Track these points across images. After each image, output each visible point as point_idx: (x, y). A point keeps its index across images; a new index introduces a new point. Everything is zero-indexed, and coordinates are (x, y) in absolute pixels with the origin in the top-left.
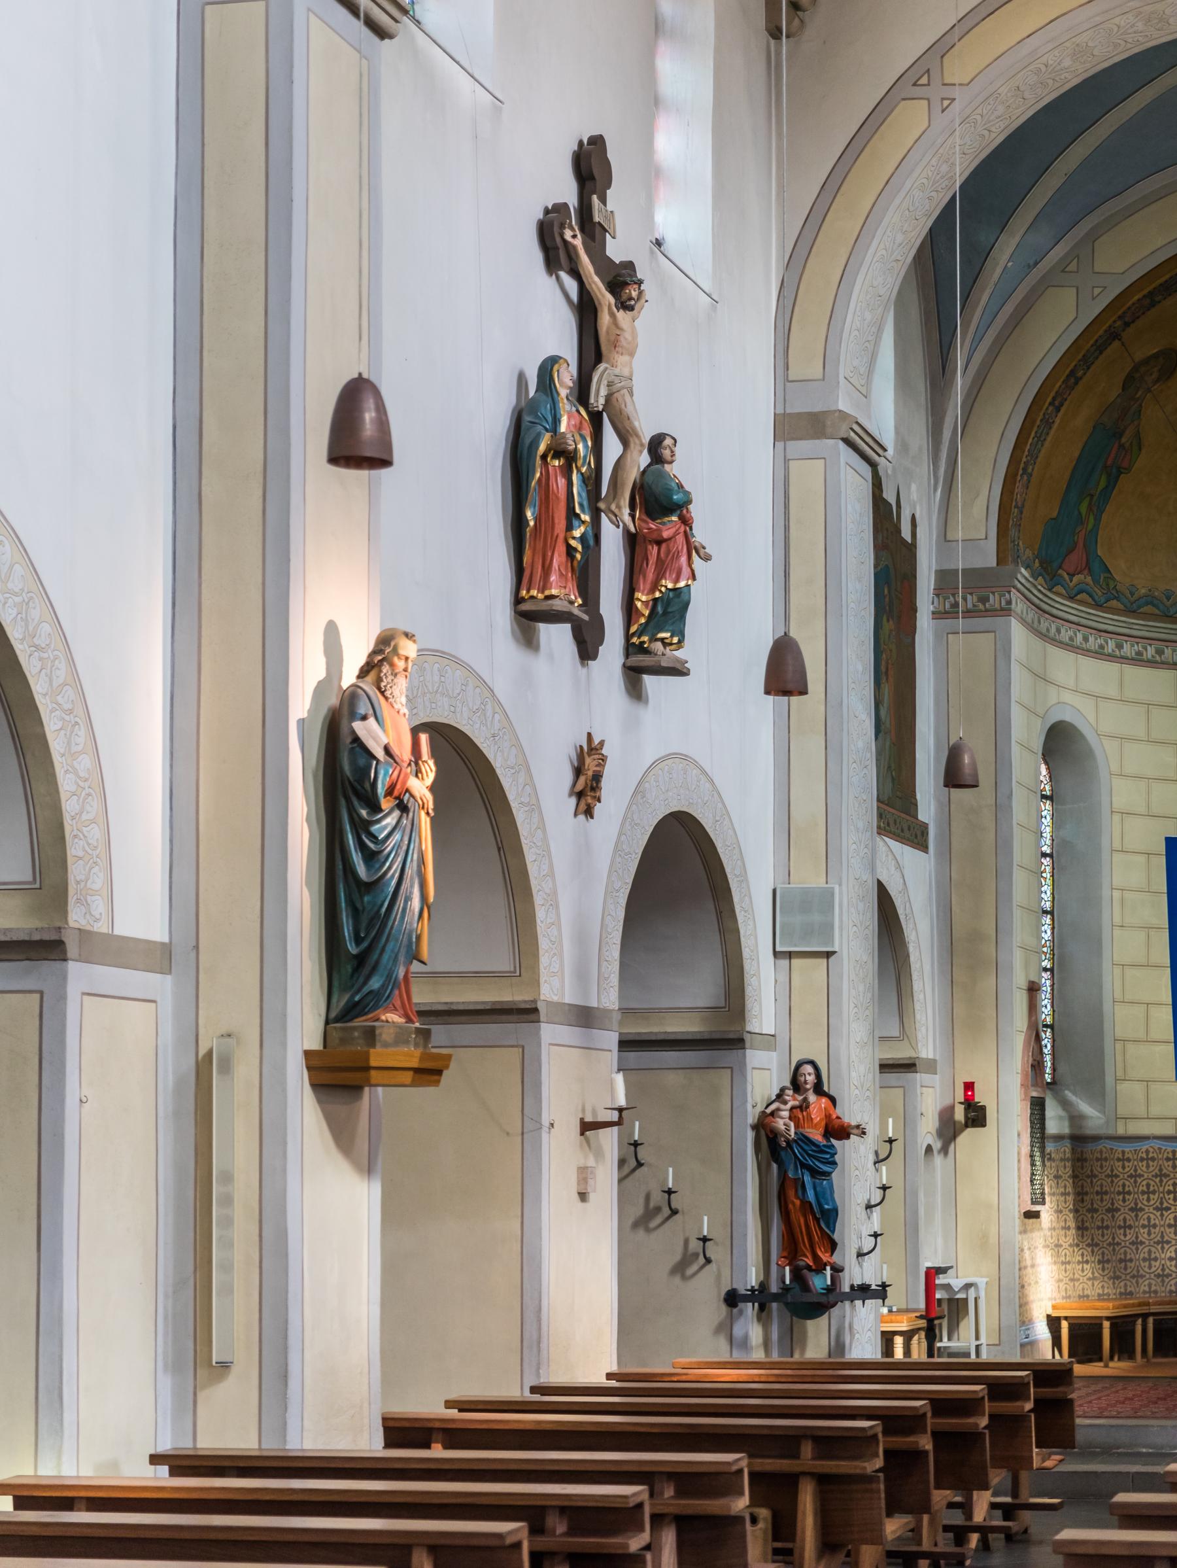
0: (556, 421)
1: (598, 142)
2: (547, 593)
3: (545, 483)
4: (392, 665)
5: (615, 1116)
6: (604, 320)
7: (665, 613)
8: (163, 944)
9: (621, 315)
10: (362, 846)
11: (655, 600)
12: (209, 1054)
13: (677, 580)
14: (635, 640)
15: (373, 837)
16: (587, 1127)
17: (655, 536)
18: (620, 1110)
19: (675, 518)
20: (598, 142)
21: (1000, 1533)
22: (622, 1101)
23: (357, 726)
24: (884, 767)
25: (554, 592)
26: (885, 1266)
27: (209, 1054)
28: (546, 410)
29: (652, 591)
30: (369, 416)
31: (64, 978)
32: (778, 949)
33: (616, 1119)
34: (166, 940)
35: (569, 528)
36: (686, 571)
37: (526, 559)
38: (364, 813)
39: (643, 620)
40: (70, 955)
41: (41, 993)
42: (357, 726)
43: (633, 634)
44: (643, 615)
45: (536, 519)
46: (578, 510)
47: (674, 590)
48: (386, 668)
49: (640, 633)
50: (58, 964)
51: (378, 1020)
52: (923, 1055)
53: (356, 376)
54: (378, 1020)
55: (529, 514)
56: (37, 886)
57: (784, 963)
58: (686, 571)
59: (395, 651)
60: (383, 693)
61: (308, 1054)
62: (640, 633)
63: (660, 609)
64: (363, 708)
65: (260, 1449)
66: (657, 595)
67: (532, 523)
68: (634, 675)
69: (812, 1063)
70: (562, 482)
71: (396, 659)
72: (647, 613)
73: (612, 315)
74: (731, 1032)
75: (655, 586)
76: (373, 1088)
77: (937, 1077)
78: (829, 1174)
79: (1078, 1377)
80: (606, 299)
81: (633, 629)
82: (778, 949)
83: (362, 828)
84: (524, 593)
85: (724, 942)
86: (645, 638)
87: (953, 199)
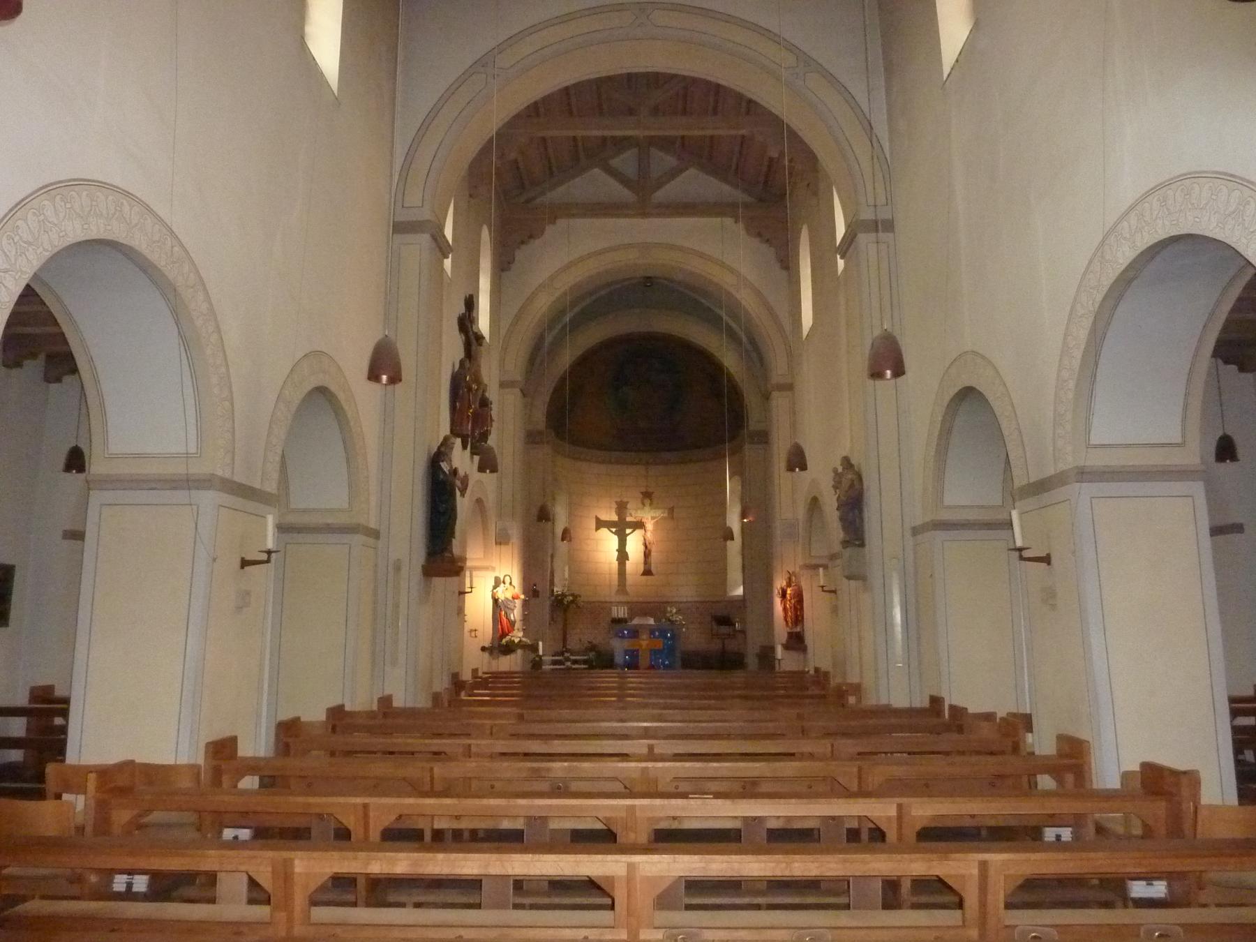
5: (264, 557)
6: (474, 348)
16: (245, 563)
18: (269, 552)
22: (270, 544)
23: (441, 463)
80: (474, 341)
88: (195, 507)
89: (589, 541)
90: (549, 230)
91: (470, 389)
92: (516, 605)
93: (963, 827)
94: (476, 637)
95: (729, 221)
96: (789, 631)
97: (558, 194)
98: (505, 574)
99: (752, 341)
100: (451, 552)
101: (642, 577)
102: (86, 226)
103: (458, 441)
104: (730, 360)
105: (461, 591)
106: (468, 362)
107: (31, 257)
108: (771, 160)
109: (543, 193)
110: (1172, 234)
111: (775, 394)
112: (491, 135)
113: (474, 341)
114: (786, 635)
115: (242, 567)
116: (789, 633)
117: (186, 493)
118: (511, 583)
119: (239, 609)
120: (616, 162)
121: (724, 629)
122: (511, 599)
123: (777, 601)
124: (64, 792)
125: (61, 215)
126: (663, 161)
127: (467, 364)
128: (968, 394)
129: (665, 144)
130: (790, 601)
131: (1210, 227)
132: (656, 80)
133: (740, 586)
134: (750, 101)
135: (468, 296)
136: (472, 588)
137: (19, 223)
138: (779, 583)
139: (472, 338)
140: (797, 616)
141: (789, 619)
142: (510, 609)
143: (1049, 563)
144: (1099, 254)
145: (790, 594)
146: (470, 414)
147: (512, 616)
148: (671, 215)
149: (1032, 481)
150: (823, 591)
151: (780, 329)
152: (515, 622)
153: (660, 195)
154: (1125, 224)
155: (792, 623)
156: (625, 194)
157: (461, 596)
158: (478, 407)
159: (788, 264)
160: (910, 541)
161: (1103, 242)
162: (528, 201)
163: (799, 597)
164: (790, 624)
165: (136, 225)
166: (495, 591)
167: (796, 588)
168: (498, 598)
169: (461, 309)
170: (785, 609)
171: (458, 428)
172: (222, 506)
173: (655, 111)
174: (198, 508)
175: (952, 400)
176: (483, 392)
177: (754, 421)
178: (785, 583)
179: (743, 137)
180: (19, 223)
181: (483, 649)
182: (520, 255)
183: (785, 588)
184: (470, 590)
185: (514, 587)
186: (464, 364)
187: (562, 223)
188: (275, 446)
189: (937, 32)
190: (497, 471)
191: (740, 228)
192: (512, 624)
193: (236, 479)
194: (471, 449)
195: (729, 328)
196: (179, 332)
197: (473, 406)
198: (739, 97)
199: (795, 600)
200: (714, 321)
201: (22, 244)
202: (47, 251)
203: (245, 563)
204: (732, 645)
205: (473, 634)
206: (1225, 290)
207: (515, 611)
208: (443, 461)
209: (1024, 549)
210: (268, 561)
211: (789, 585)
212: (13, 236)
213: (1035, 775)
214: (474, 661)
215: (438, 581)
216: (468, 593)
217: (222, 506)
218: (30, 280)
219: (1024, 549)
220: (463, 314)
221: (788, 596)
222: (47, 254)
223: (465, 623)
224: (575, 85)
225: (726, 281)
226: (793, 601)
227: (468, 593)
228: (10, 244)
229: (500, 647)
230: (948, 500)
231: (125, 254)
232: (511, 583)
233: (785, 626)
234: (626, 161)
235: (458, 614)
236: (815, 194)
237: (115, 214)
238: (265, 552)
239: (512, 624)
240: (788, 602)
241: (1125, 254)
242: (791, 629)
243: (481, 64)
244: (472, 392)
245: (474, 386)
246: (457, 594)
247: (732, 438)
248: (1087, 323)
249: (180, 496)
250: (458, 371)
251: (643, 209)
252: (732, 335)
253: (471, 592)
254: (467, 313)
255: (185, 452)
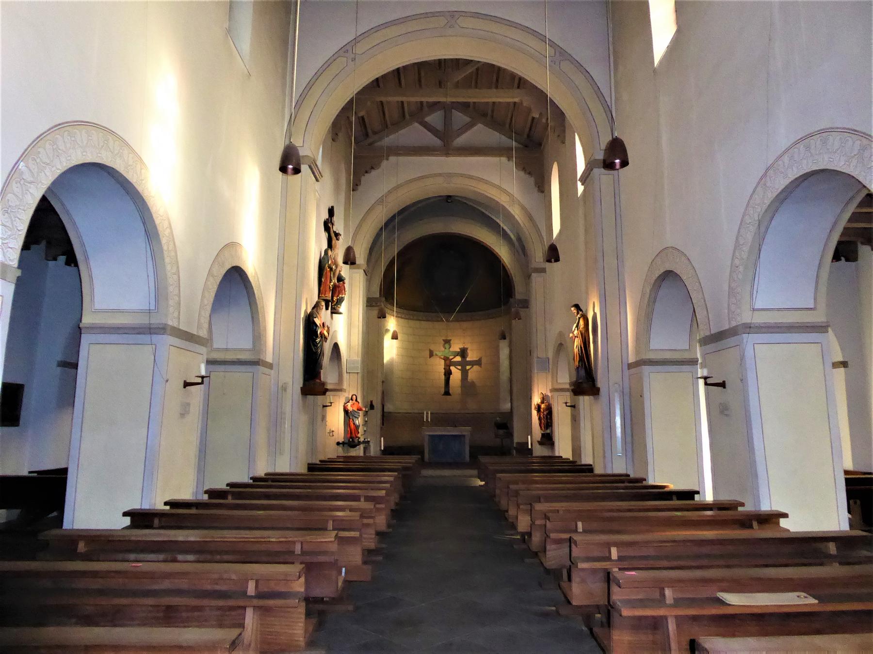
1: (332, 207)
5: (199, 380)
6: (333, 242)
16: (187, 384)
18: (203, 377)
20: (332, 207)
21: (388, 484)
22: (203, 373)
23: (315, 319)
24: (605, 566)
26: (530, 447)
33: (200, 381)
35: (330, 282)
42: (315, 319)
52: (170, 323)
68: (332, 313)
77: (273, 371)
79: (141, 506)
88: (154, 346)
90: (385, 163)
91: (331, 269)
94: (333, 436)
95: (504, 159)
96: (543, 432)
97: (390, 140)
98: (353, 394)
99: (519, 239)
101: (444, 396)
102: (84, 154)
103: (323, 304)
104: (503, 252)
107: (48, 174)
108: (533, 118)
109: (380, 139)
110: (814, 169)
111: (534, 275)
112: (352, 96)
114: (541, 434)
115: (185, 387)
116: (542, 434)
117: (149, 336)
118: (356, 400)
119: (182, 415)
120: (428, 119)
122: (356, 410)
123: (534, 413)
125: (68, 145)
126: (459, 118)
127: (330, 252)
128: (668, 276)
129: (465, 107)
130: (543, 413)
131: (839, 164)
132: (458, 64)
134: (520, 79)
137: (39, 150)
138: (536, 400)
139: (333, 235)
140: (547, 423)
142: (356, 417)
143: (724, 387)
144: (762, 182)
147: (357, 422)
148: (466, 155)
149: (713, 332)
150: (567, 406)
151: (538, 231)
152: (359, 425)
153: (462, 140)
154: (780, 163)
155: (544, 428)
156: (436, 141)
158: (336, 281)
159: (543, 187)
160: (626, 372)
161: (765, 175)
162: (370, 144)
163: (549, 410)
165: (118, 153)
167: (547, 404)
169: (325, 215)
170: (540, 419)
171: (323, 295)
173: (457, 86)
174: (156, 347)
175: (656, 280)
176: (340, 271)
178: (539, 401)
179: (515, 103)
180: (39, 150)
181: (338, 444)
182: (365, 179)
183: (540, 404)
185: (359, 403)
188: (206, 306)
189: (651, 31)
191: (513, 164)
192: (357, 427)
194: (331, 310)
196: (145, 230)
197: (333, 281)
199: (547, 412)
200: (494, 227)
201: (41, 164)
202: (59, 169)
203: (187, 384)
205: (331, 434)
206: (842, 211)
207: (359, 419)
208: (315, 318)
209: (709, 378)
210: (202, 383)
211: (542, 402)
212: (36, 158)
213: (752, 520)
214: (331, 451)
215: (310, 398)
216: (329, 406)
218: (46, 192)
219: (709, 378)
220: (327, 219)
221: (542, 410)
222: (59, 171)
224: (404, 67)
225: (503, 200)
226: (545, 413)
227: (329, 406)
228: (34, 164)
229: (350, 441)
230: (654, 345)
231: (109, 173)
232: (356, 400)
233: (540, 429)
234: (435, 118)
235: (322, 420)
236: (563, 143)
237: (103, 146)
238: (200, 377)
240: (542, 413)
241: (781, 183)
243: (344, 50)
245: (334, 267)
248: (753, 229)
249: (146, 338)
251: (447, 149)
252: (505, 236)
253: (331, 406)
255: (148, 309)
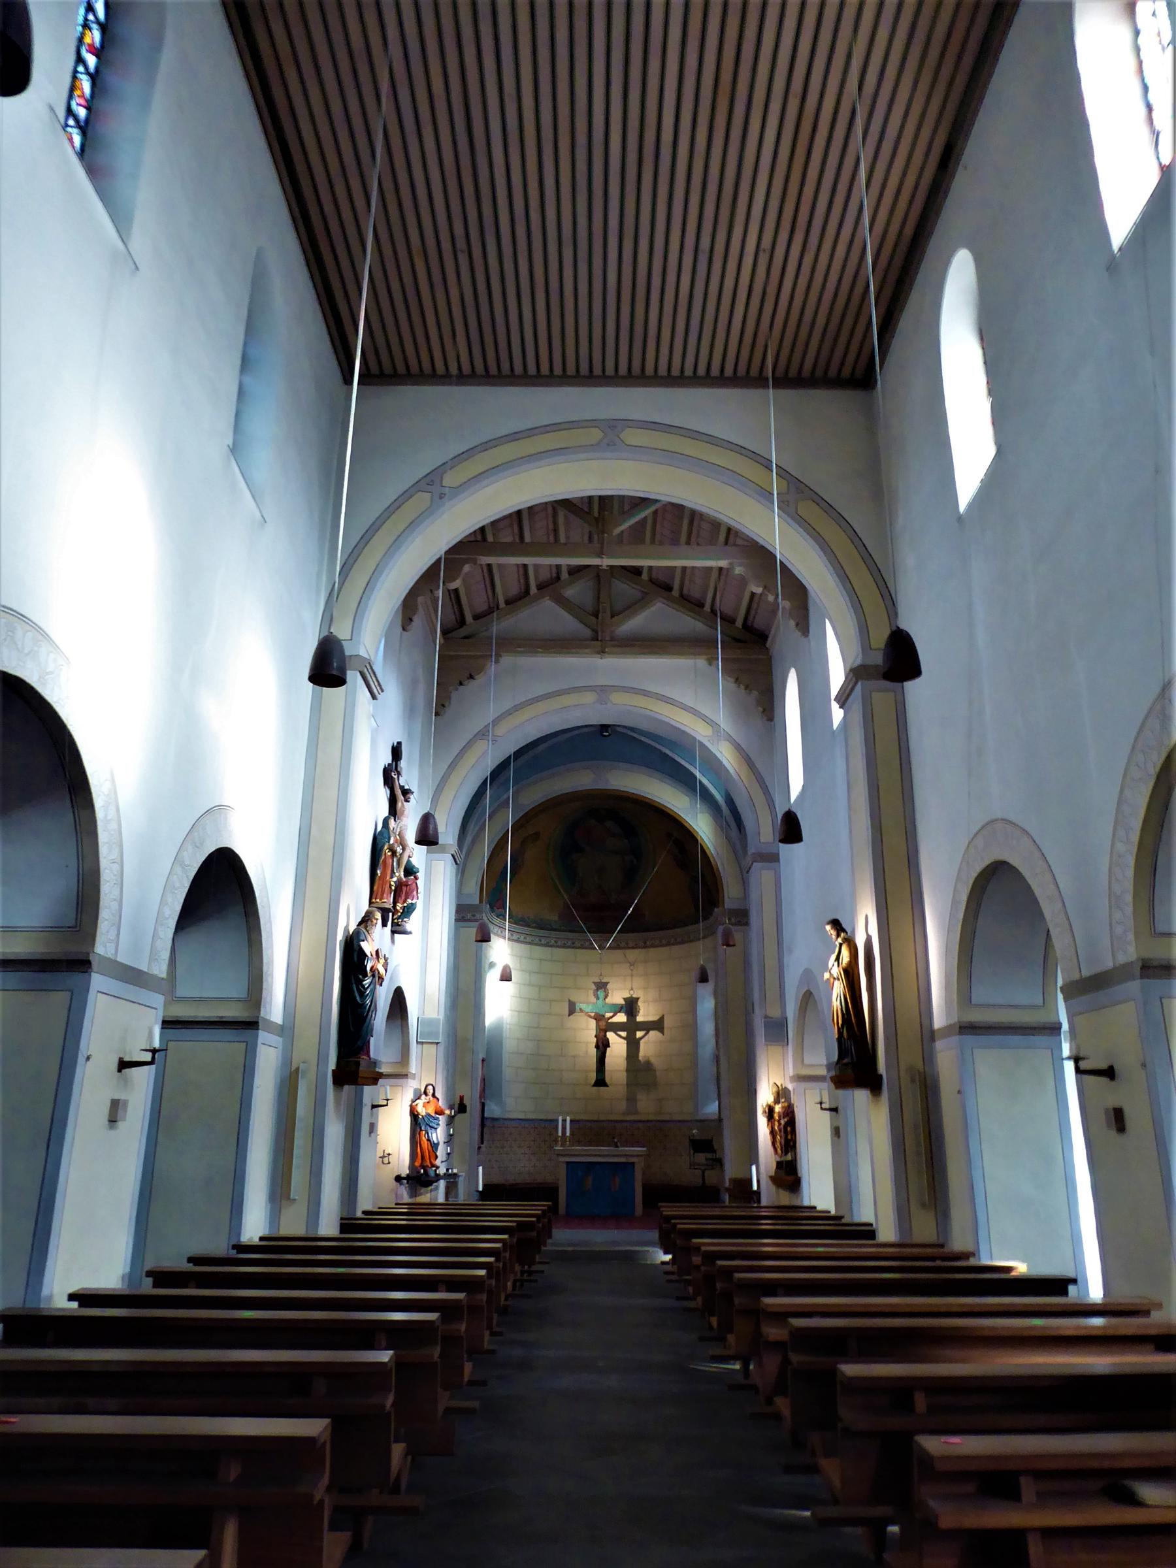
0: (389, 839)
2: (383, 901)
3: (385, 861)
4: (372, 921)
5: (148, 1057)
6: (399, 804)
7: (408, 912)
8: (280, 1025)
9: (405, 803)
10: (359, 990)
11: (404, 907)
12: (298, 1069)
13: (412, 900)
14: (396, 921)
15: (363, 986)
16: (123, 1065)
17: (405, 883)
19: (412, 877)
20: (399, 743)
25: (385, 900)
27: (298, 1069)
28: (386, 835)
29: (404, 903)
30: (431, 827)
31: (257, 1036)
32: (419, 1040)
34: (282, 1024)
35: (392, 877)
36: (416, 897)
37: (375, 888)
38: (361, 977)
39: (399, 914)
40: (260, 1027)
41: (247, 1042)
42: (362, 943)
43: (395, 919)
44: (399, 912)
45: (381, 874)
46: (395, 871)
47: (412, 903)
48: (369, 923)
49: (398, 919)
50: (256, 1031)
51: (360, 1058)
53: (787, 810)
54: (360, 1058)
55: (379, 872)
56: (249, 999)
57: (420, 1046)
58: (416, 897)
59: (374, 916)
60: (368, 931)
61: (333, 1070)
62: (398, 919)
63: (406, 909)
64: (362, 937)
65: (307, 1234)
66: (405, 905)
67: (379, 875)
69: (432, 1085)
70: (391, 861)
71: (373, 920)
72: (401, 911)
73: (402, 803)
74: (403, 1071)
75: (405, 901)
76: (358, 1087)
78: (436, 1129)
80: (400, 797)
81: (395, 917)
82: (419, 1040)
83: (360, 982)
84: (374, 900)
85: (403, 1036)
86: (400, 920)
87: (487, 778)
89: (400, 1020)
91: (394, 853)
92: (440, 1122)
93: (772, 675)
96: (778, 1159)
100: (368, 1055)
105: (834, 1113)
106: (392, 820)
113: (400, 797)
115: (120, 1070)
116: (778, 1163)
118: (434, 1095)
121: (701, 1157)
124: (76, 1309)
126: (623, 589)
127: (392, 823)
133: (715, 1101)
135: (395, 744)
136: (387, 1100)
139: (399, 792)
141: (778, 1145)
142: (432, 1127)
145: (779, 1112)
146: (392, 883)
152: (438, 1144)
155: (781, 1149)
157: (375, 1110)
158: (402, 875)
164: (779, 1151)
166: (414, 1104)
167: (786, 1104)
168: (418, 1114)
170: (773, 1133)
172: (100, 992)
177: (731, 892)
179: (721, 569)
181: (398, 1179)
183: (772, 1104)
184: (385, 1103)
185: (438, 1100)
186: (388, 824)
187: (507, 660)
190: (511, 980)
193: (119, 959)
195: (704, 790)
197: (397, 874)
198: (716, 525)
199: (786, 1120)
200: (686, 781)
203: (123, 1065)
204: (711, 1177)
205: (386, 1160)
211: (777, 1101)
217: (100, 992)
221: (776, 1116)
223: (378, 1145)
226: (782, 1122)
232: (434, 1095)
239: (435, 1146)
242: (781, 1157)
244: (396, 856)
245: (399, 850)
246: (370, 1107)
247: (705, 918)
250: (380, 831)
252: (706, 796)
253: (387, 1105)
254: (394, 763)
